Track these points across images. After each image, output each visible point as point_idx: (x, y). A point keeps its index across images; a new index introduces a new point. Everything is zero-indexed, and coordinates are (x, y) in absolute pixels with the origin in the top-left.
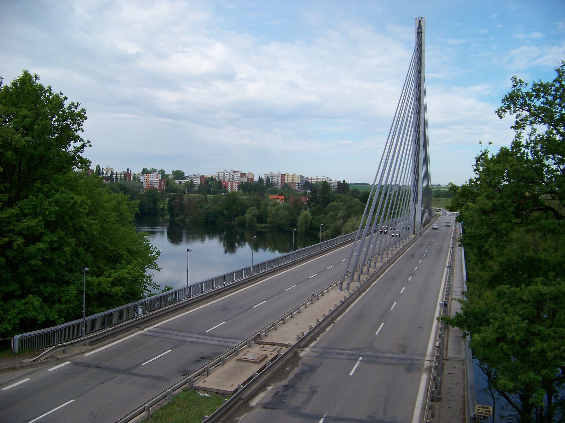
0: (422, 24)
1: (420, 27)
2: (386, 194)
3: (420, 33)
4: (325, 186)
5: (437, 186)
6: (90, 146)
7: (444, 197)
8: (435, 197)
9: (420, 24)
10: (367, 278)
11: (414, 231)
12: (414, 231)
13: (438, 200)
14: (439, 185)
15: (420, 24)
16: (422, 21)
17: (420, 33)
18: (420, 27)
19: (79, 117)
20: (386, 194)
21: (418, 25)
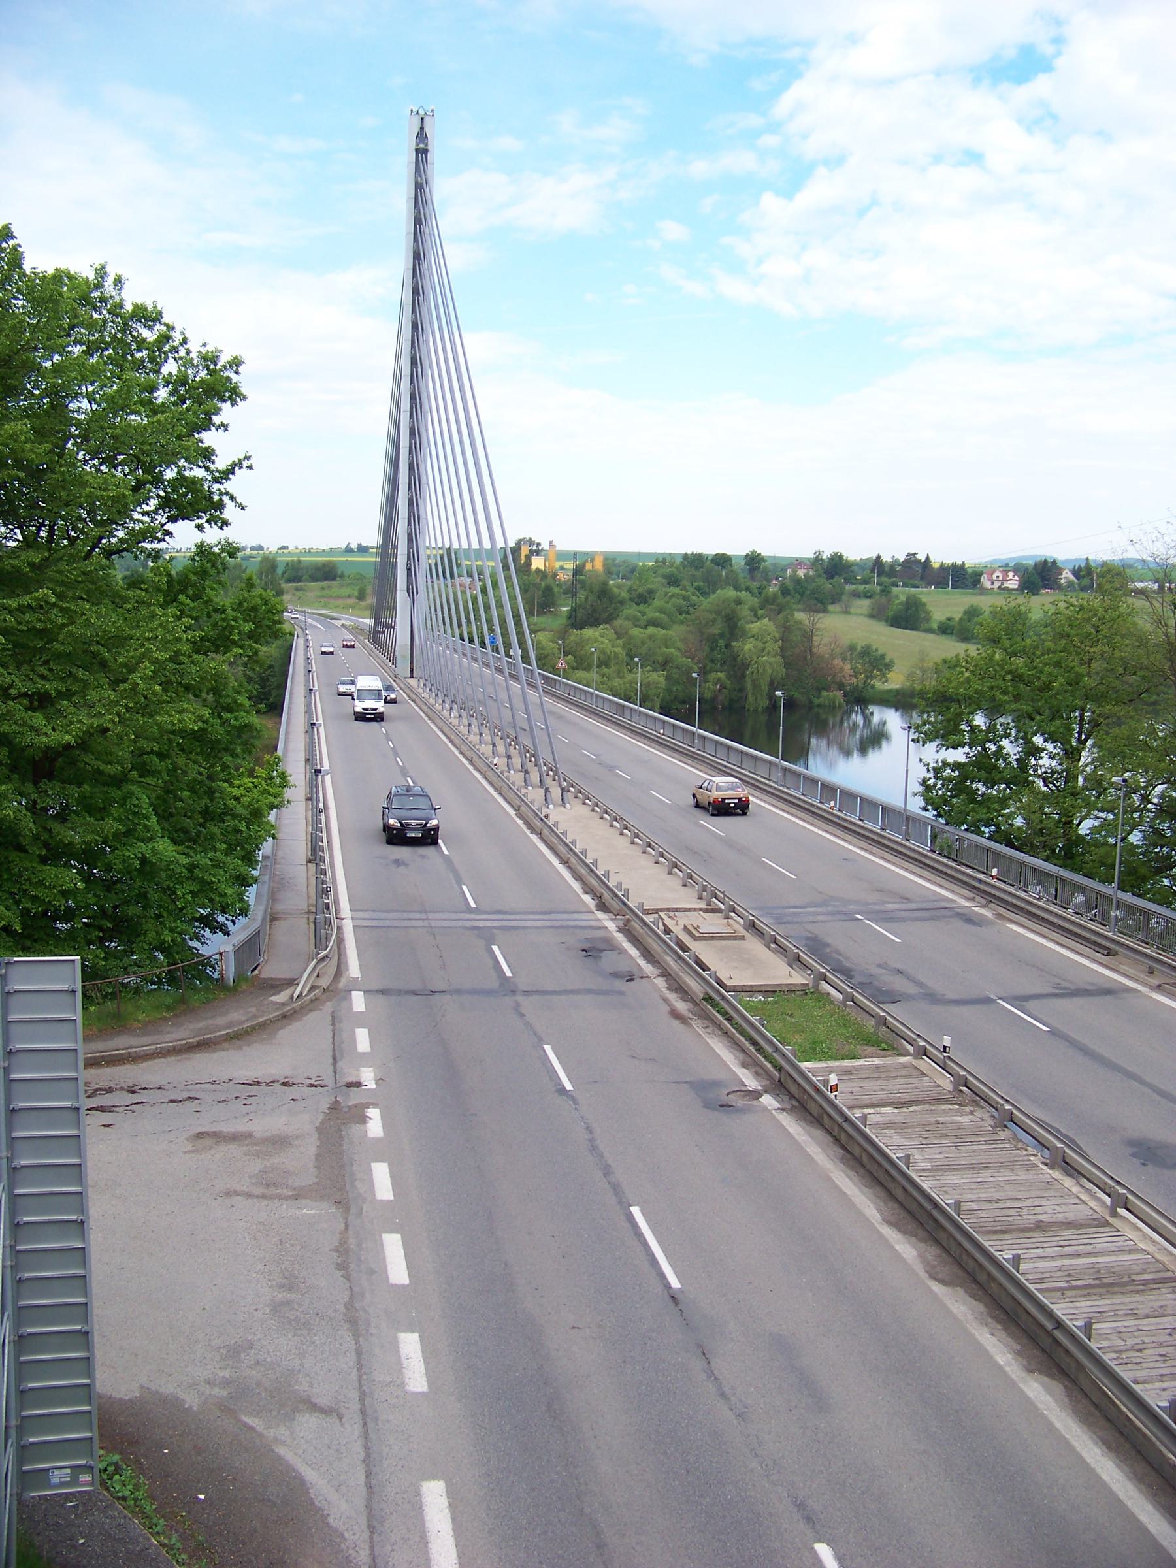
0: (427, 129)
1: (422, 136)
2: (445, 577)
3: (422, 153)
4: (722, 560)
5: (252, 549)
6: (250, 467)
7: (314, 579)
8: (289, 581)
9: (422, 128)
10: (533, 802)
11: (412, 671)
12: (412, 671)
13: (297, 589)
14: (260, 548)
15: (422, 128)
16: (427, 120)
17: (422, 153)
18: (422, 136)
19: (212, 389)
20: (445, 577)
21: (416, 130)
